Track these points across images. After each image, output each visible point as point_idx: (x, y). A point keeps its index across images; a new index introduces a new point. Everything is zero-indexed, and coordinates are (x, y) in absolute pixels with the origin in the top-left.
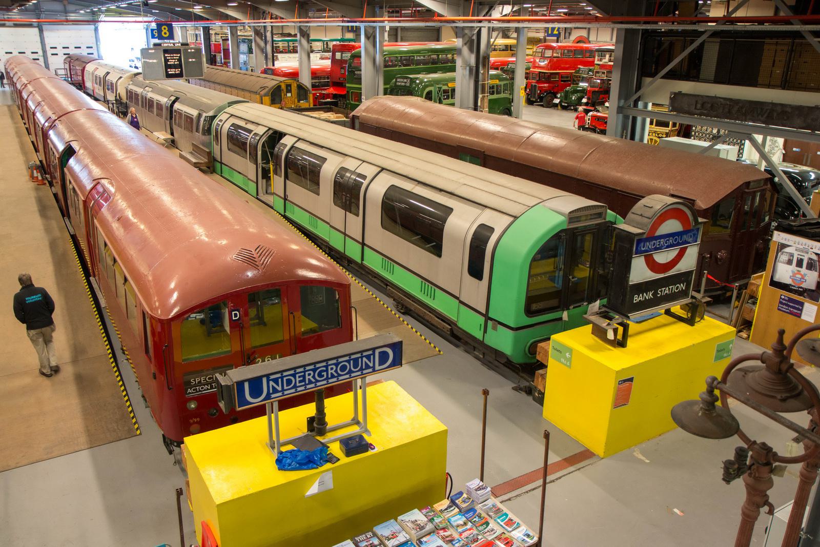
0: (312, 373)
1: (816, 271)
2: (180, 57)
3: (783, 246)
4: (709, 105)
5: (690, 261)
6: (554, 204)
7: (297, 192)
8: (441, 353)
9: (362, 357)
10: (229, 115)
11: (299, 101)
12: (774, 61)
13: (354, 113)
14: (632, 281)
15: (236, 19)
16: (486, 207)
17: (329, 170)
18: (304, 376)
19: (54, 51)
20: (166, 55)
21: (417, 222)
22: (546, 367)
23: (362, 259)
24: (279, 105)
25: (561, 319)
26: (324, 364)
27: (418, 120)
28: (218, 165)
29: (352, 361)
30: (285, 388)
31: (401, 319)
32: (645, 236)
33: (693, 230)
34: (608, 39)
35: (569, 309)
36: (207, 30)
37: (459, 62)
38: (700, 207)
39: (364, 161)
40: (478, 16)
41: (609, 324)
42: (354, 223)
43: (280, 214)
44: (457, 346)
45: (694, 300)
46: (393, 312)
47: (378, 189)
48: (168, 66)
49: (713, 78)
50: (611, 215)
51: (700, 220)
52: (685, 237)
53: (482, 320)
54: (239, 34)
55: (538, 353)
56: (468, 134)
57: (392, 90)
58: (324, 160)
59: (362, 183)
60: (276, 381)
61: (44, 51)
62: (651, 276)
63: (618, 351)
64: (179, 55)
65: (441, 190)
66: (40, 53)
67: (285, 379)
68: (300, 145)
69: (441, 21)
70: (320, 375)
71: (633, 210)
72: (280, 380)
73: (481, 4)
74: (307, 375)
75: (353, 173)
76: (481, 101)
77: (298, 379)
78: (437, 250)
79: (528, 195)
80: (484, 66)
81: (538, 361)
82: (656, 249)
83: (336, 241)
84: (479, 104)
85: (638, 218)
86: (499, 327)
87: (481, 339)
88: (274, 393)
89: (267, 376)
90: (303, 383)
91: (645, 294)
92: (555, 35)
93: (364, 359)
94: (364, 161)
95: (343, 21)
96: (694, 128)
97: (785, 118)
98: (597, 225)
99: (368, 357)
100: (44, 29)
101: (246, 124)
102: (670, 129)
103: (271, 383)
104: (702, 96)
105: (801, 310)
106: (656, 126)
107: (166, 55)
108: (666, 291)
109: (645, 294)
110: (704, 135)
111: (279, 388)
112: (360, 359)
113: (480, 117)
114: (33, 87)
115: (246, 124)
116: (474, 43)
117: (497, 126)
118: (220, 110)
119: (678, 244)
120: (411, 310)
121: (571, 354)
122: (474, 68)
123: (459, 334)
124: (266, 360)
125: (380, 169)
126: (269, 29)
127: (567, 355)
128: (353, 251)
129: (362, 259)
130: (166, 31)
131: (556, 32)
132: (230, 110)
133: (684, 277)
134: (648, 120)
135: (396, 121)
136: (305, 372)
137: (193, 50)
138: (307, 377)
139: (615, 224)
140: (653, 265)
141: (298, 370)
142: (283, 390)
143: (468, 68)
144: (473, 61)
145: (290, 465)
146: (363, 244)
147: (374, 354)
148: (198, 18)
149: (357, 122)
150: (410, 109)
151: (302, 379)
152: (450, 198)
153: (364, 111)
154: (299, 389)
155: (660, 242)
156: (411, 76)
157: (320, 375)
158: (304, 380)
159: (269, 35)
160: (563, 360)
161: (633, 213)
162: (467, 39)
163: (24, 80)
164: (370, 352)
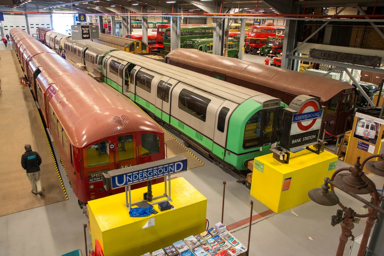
0: (156, 170)
1: (375, 130)
2: (89, 29)
3: (360, 119)
4: (327, 55)
5: (318, 125)
6: (257, 98)
7: (141, 91)
8: (205, 165)
9: (169, 166)
10: (111, 56)
11: (142, 50)
12: (357, 35)
13: (167, 56)
14: (291, 134)
15: (114, 13)
16: (226, 99)
17: (155, 82)
18: (142, 175)
19: (32, 26)
20: (82, 29)
21: (195, 106)
22: (252, 172)
23: (170, 122)
24: (133, 52)
25: (259, 150)
26: (152, 169)
27: (196, 59)
28: (105, 79)
29: (164, 168)
30: (134, 179)
31: (187, 149)
32: (297, 114)
33: (319, 111)
34: (282, 24)
35: (263, 146)
36: (101, 18)
37: (215, 34)
38: (323, 101)
39: (171, 78)
40: (223, 13)
41: (281, 153)
42: (166, 105)
43: (133, 101)
44: (212, 162)
45: (319, 143)
46: (183, 146)
47: (177, 90)
48: (83, 34)
49: (329, 43)
50: (282, 104)
51: (323, 106)
52: (316, 114)
53: (223, 150)
54: (116, 19)
55: (248, 166)
56: (218, 66)
57: (184, 46)
58: (153, 77)
59: (170, 88)
60: (130, 176)
61: (28, 26)
62: (300, 131)
63: (285, 165)
64: (88, 29)
65: (206, 91)
66: (26, 27)
67: (134, 175)
68: (142, 70)
69: (207, 15)
70: (150, 174)
71: (292, 102)
72: (132, 176)
73: (225, 8)
74: (144, 174)
75: (166, 83)
76: (224, 51)
77: (140, 176)
78: (204, 118)
79: (245, 94)
80: (226, 35)
81: (248, 169)
82: (302, 119)
83: (158, 114)
84: (223, 53)
85: (295, 105)
86: (231, 153)
87: (223, 159)
88: (129, 182)
89: (126, 174)
90: (142, 178)
91: (297, 140)
92: (258, 22)
93: (170, 167)
94: (171, 78)
95: (163, 15)
96: (320, 65)
97: (362, 61)
98: (276, 108)
99: (172, 166)
100: (28, 16)
101: (118, 60)
102: (309, 65)
103: (128, 177)
104: (324, 51)
105: (368, 148)
106: (303, 64)
107: (82, 29)
108: (307, 138)
109: (297, 140)
110: (325, 68)
111: (131, 180)
112: (168, 167)
113: (224, 59)
114: (22, 42)
115: (118, 60)
116: (221, 25)
117: (231, 63)
118: (107, 53)
119: (313, 117)
120: (191, 145)
121: (263, 166)
122: (222, 37)
123: (213, 157)
124: (125, 167)
125: (178, 81)
126: (129, 17)
127: (262, 166)
128: (166, 118)
129: (170, 122)
130: (83, 18)
131: (258, 21)
132: (111, 54)
133: (315, 132)
134: (300, 61)
135: (186, 60)
136: (143, 172)
137: (95, 27)
138: (144, 175)
139: (284, 108)
140: (301, 127)
141: (140, 172)
142: (133, 181)
143: (219, 37)
144: (221, 33)
145: (135, 214)
146: (170, 115)
147: (174, 165)
148: (97, 12)
149: (168, 60)
150: (192, 54)
151: (141, 175)
152: (210, 95)
153: (171, 55)
154: (140, 180)
155: (304, 116)
156: (193, 40)
157: (150, 174)
158: (142, 176)
159: (129, 20)
160: (259, 169)
161: (292, 103)
162: (218, 23)
163: (18, 39)
164: (173, 164)
